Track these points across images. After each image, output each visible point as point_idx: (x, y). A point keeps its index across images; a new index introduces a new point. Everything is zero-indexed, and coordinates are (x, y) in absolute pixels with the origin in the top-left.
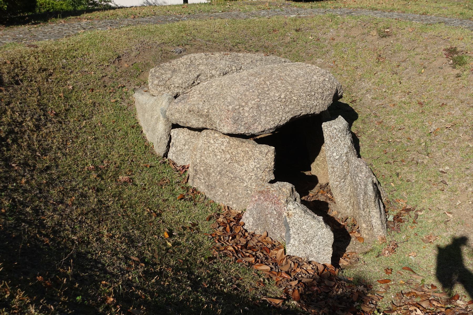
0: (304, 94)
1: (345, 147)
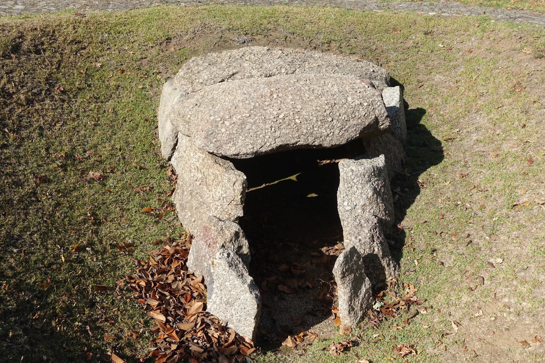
0: (315, 119)
1: (362, 197)
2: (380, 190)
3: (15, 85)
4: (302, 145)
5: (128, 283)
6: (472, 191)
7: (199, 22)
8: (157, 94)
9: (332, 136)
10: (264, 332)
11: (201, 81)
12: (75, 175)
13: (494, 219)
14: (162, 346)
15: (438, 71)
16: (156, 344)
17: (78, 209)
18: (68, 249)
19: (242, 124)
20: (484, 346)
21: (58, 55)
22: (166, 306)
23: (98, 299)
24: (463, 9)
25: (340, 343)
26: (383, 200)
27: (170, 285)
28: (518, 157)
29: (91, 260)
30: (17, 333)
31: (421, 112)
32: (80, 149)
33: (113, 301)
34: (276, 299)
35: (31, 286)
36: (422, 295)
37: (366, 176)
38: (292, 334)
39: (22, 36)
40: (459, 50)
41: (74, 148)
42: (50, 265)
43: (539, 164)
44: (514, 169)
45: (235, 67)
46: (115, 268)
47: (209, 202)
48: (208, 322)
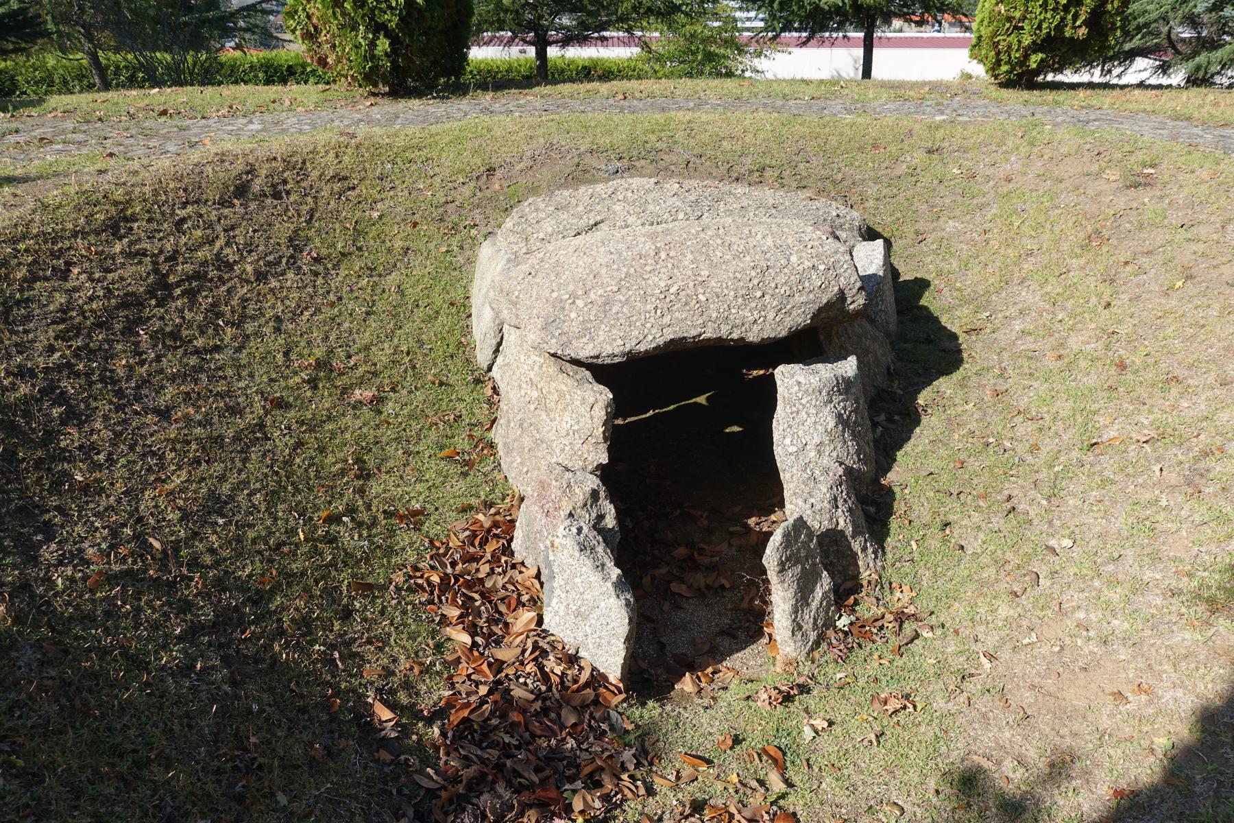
0: (732, 293)
2: (849, 417)
3: (238, 250)
4: (709, 340)
5: (410, 577)
6: (1015, 420)
7: (542, 141)
8: (471, 261)
9: (762, 323)
10: (644, 665)
11: (541, 235)
12: (330, 395)
13: (1056, 469)
14: (463, 689)
15: (952, 215)
16: (452, 684)
17: (333, 451)
18: (311, 519)
19: (605, 304)
20: (1040, 698)
21: (309, 199)
22: (474, 618)
23: (358, 605)
24: (994, 110)
25: (775, 688)
26: (855, 436)
27: (481, 581)
28: (1099, 359)
29: (350, 539)
30: (211, 663)
31: (922, 285)
32: (341, 353)
33: (384, 608)
34: (666, 607)
35: (243, 582)
36: (924, 605)
37: (824, 393)
38: (692, 668)
39: (251, 171)
40: (988, 178)
41: (331, 351)
42: (279, 545)
43: (1138, 371)
44: (1091, 381)
45: (599, 212)
46: (390, 551)
47: (553, 438)
48: (546, 646)
